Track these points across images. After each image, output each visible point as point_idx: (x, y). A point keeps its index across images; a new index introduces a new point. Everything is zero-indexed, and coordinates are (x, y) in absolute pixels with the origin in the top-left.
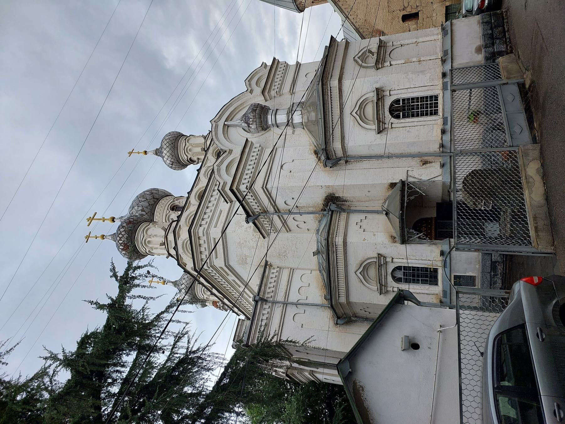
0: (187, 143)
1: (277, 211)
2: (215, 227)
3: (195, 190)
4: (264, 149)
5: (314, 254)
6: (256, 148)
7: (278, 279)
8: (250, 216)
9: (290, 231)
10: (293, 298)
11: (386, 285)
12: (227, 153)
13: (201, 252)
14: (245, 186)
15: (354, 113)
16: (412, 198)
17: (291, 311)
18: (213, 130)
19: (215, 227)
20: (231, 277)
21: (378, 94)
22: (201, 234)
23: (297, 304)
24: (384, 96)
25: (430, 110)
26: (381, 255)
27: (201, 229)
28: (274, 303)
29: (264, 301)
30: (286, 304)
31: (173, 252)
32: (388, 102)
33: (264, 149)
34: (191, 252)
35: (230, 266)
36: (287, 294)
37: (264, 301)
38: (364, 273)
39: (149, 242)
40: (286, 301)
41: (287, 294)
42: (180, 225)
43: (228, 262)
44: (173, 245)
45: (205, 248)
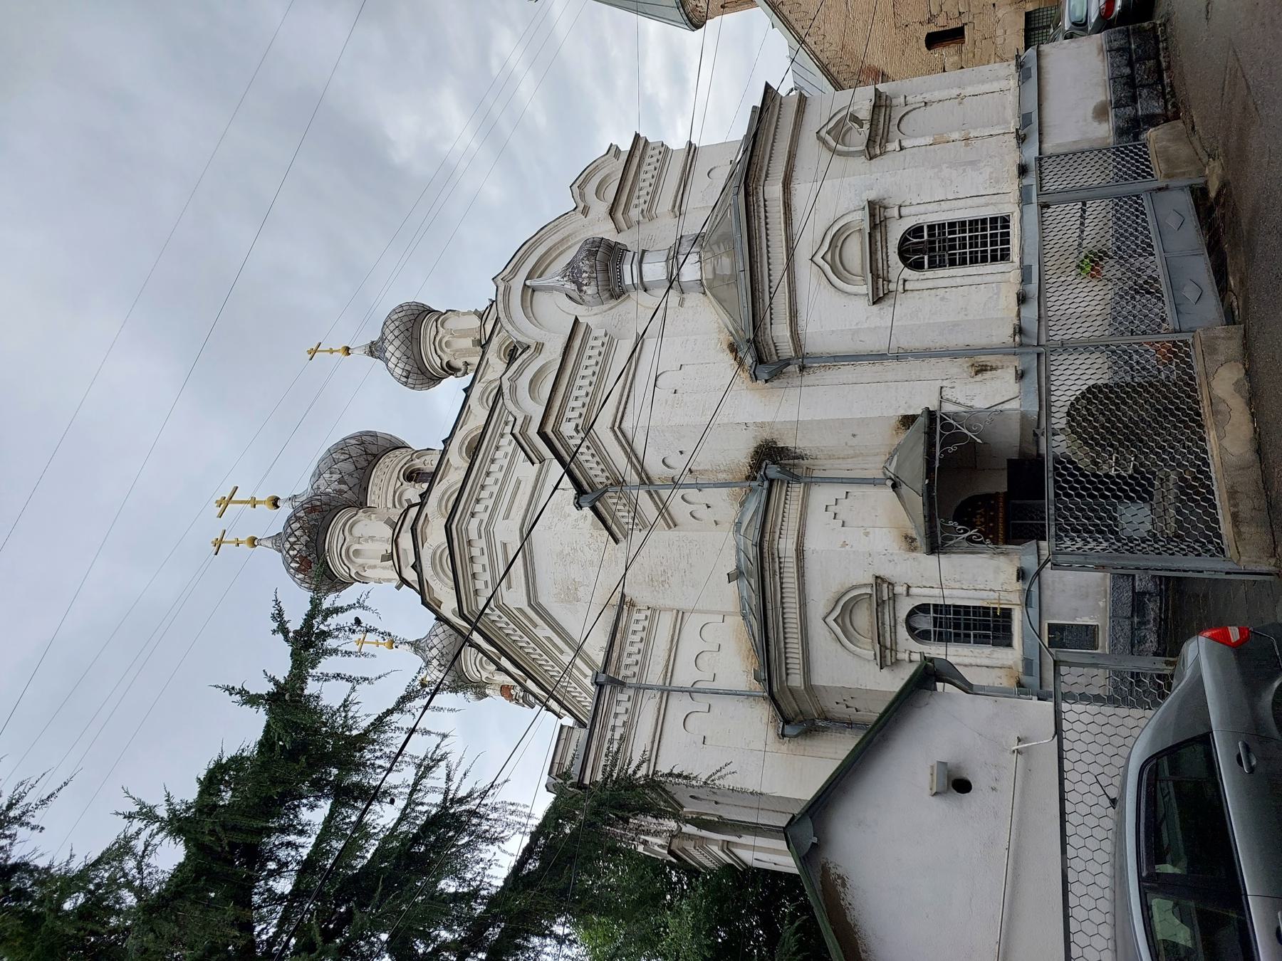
0: (441, 329)
1: (646, 480)
2: (506, 517)
3: (459, 435)
4: (616, 340)
5: (730, 578)
6: (596, 338)
7: (645, 657)
8: (585, 493)
9: (675, 526)
10: (683, 677)
11: (894, 648)
12: (532, 350)
13: (474, 575)
14: (572, 424)
15: (818, 259)
16: (952, 449)
17: (679, 705)
18: (500, 298)
19: (506, 517)
20: (543, 631)
21: (872, 215)
22: (473, 535)
23: (691, 692)
24: (886, 218)
25: (992, 251)
26: (883, 580)
27: (474, 523)
28: (640, 688)
29: (619, 684)
30: (666, 691)
31: (411, 575)
32: (896, 232)
33: (616, 340)
34: (451, 575)
35: (539, 605)
36: (669, 669)
37: (619, 684)
38: (843, 621)
39: (357, 552)
40: (667, 684)
41: (669, 669)
42: (448, 460)
43: (536, 597)
44: (412, 560)
45: (484, 566)
